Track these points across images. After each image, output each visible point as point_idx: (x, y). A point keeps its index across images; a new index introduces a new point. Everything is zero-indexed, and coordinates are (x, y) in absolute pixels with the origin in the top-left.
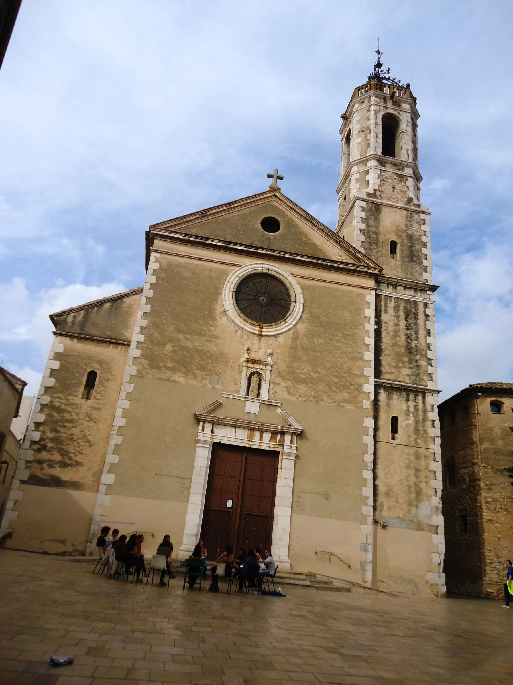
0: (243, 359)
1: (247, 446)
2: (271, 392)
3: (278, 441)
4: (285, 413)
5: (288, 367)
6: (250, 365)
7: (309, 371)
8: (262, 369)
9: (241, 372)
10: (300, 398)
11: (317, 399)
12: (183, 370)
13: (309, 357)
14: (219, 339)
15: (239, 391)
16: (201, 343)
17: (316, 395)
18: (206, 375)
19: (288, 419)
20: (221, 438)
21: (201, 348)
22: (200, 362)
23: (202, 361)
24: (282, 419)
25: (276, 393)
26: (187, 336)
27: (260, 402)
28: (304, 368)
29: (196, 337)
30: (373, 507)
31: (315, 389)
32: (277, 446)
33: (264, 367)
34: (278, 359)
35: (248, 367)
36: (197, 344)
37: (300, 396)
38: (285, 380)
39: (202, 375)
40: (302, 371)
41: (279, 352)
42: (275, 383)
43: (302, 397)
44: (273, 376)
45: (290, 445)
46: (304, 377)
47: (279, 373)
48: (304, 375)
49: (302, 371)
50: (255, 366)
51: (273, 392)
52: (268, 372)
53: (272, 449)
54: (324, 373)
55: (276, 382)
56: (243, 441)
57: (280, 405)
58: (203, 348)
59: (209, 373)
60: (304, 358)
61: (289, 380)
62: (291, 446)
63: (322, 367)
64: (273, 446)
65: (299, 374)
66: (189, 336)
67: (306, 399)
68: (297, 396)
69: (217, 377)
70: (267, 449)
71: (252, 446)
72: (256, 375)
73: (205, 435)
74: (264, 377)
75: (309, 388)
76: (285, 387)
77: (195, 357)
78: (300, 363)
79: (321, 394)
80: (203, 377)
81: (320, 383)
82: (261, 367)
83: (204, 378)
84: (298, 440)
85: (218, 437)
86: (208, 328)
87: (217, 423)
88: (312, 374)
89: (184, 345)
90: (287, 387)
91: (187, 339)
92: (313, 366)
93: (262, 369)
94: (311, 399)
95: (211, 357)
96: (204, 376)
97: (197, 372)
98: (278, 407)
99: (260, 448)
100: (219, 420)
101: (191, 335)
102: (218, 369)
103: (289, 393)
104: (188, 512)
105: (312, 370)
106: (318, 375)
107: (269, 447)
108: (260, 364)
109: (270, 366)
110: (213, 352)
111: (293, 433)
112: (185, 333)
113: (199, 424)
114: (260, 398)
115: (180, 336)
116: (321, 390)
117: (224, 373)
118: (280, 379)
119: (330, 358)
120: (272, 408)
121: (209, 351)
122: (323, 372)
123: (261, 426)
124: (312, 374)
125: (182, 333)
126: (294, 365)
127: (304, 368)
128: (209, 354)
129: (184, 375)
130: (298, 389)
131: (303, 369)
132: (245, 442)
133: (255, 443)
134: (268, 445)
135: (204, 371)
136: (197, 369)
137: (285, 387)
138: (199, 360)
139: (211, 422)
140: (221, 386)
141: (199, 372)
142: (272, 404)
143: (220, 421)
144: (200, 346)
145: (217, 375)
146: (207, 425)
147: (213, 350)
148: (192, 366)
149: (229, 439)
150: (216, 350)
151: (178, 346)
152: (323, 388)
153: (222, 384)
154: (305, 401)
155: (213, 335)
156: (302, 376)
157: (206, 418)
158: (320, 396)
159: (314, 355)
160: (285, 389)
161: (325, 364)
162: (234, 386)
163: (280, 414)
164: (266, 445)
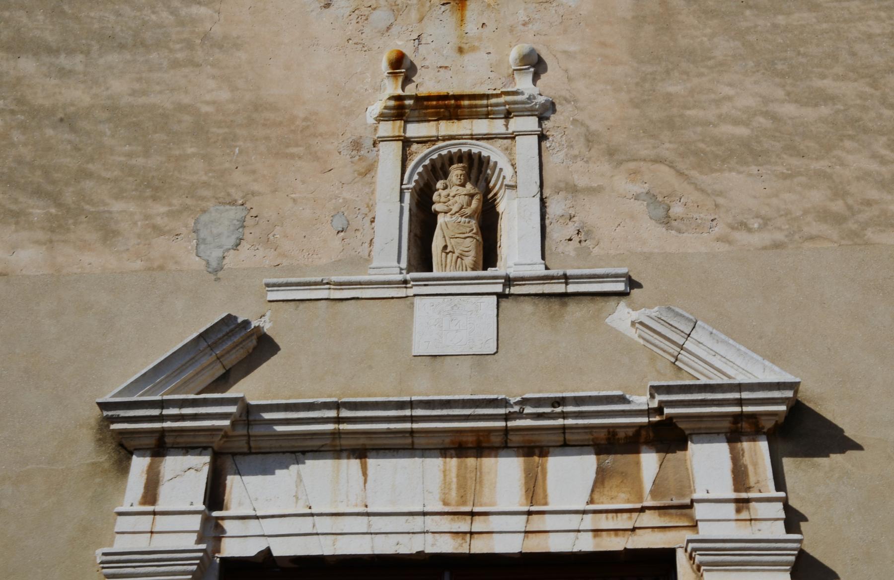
0: (377, 107)
1: (446, 546)
2: (556, 233)
3: (648, 485)
4: (659, 319)
5: (635, 104)
6: (415, 130)
7: (766, 100)
8: (488, 138)
9: (369, 170)
10: (741, 237)
11: (852, 225)
12: (38, 210)
13: (752, 38)
14: (237, 46)
15: (369, 258)
16: (139, 80)
17: (838, 206)
18: (171, 214)
19: (689, 345)
20: (269, 526)
21: (142, 100)
22: (140, 161)
23: (146, 154)
24: (653, 358)
25: (588, 233)
26: (63, 60)
27: (499, 289)
28: (730, 91)
29: (113, 58)
30: (583, 514)
31: (822, 175)
32: (649, 519)
33: (497, 126)
34: (570, 79)
35: (407, 143)
36: (119, 86)
37: (743, 226)
38: (632, 165)
39: (147, 217)
40: (725, 108)
41: (573, 48)
42: (573, 190)
43: (750, 230)
44: (553, 160)
45: (733, 495)
46: (742, 131)
47: (590, 139)
48: (736, 122)
49: (725, 108)
50: (446, 128)
51: (571, 230)
52: (527, 146)
53: (615, 544)
54: (862, 96)
55: (581, 181)
56: (417, 523)
57: (620, 287)
58: (153, 99)
59: (189, 201)
60: (724, 47)
61: (658, 160)
62: (742, 504)
63: (839, 70)
64: (624, 521)
65: (707, 123)
66: (77, 62)
67: (780, 236)
68: (718, 230)
69: (234, 213)
70: (586, 544)
71: (480, 546)
72: (456, 172)
73: (162, 523)
74: (508, 171)
75: (785, 177)
76: (637, 197)
77: (108, 141)
78: (700, 75)
79: (873, 194)
80: (155, 227)
81: (848, 144)
82: (481, 126)
83: (158, 231)
84: (788, 463)
85: (253, 527)
86: (174, 12)
87: (242, 445)
88: (789, 110)
89: (47, 103)
90: (651, 197)
91: (64, 73)
92: (782, 75)
93: (488, 138)
94: (816, 228)
95: (199, 130)
96: (159, 221)
97: (117, 206)
98: (612, 301)
99: (536, 545)
100: (248, 424)
101: (87, 53)
102: (238, 177)
103: (666, 221)
104: (468, 552)
105: (780, 93)
106: (825, 111)
107: (596, 532)
108: (474, 115)
109: (530, 112)
110: (205, 109)
111: (738, 418)
112: (52, 51)
113: (122, 467)
114: (500, 269)
115: (27, 65)
116: (864, 176)
117: (275, 191)
118: (604, 167)
119: (878, 18)
120: (575, 311)
121: (181, 108)
122: (849, 89)
123: (520, 415)
124: (789, 110)
125: (36, 55)
126: (672, 89)
127: (730, 91)
128: (187, 118)
129: (41, 235)
130: (720, 194)
131: (729, 98)
132: (432, 523)
133: (495, 523)
134: (589, 522)
135: (155, 199)
136: (118, 197)
137: (637, 197)
138: (130, 155)
139: (202, 440)
140: (261, 253)
141: (132, 207)
142: (572, 288)
143: (256, 431)
144: (133, 93)
145: (233, 203)
146: (172, 464)
147: (208, 97)
148: (88, 184)
149: (324, 524)
150: (224, 95)
151: (13, 112)
152: (874, 166)
153: (266, 241)
154: (777, 246)
155: (205, 37)
156: (727, 129)
157: (161, 418)
158: (868, 203)
159: (775, 26)
160: (640, 207)
161: (853, 54)
162: (336, 242)
163: (633, 334)
164: (573, 522)
